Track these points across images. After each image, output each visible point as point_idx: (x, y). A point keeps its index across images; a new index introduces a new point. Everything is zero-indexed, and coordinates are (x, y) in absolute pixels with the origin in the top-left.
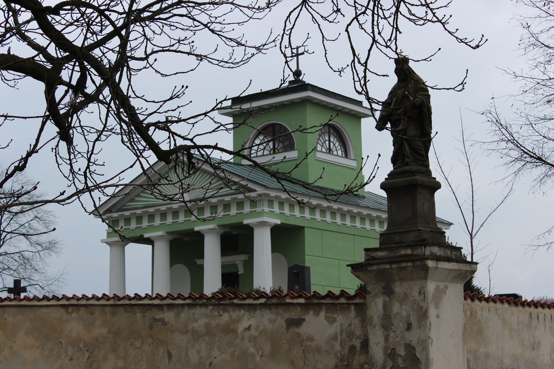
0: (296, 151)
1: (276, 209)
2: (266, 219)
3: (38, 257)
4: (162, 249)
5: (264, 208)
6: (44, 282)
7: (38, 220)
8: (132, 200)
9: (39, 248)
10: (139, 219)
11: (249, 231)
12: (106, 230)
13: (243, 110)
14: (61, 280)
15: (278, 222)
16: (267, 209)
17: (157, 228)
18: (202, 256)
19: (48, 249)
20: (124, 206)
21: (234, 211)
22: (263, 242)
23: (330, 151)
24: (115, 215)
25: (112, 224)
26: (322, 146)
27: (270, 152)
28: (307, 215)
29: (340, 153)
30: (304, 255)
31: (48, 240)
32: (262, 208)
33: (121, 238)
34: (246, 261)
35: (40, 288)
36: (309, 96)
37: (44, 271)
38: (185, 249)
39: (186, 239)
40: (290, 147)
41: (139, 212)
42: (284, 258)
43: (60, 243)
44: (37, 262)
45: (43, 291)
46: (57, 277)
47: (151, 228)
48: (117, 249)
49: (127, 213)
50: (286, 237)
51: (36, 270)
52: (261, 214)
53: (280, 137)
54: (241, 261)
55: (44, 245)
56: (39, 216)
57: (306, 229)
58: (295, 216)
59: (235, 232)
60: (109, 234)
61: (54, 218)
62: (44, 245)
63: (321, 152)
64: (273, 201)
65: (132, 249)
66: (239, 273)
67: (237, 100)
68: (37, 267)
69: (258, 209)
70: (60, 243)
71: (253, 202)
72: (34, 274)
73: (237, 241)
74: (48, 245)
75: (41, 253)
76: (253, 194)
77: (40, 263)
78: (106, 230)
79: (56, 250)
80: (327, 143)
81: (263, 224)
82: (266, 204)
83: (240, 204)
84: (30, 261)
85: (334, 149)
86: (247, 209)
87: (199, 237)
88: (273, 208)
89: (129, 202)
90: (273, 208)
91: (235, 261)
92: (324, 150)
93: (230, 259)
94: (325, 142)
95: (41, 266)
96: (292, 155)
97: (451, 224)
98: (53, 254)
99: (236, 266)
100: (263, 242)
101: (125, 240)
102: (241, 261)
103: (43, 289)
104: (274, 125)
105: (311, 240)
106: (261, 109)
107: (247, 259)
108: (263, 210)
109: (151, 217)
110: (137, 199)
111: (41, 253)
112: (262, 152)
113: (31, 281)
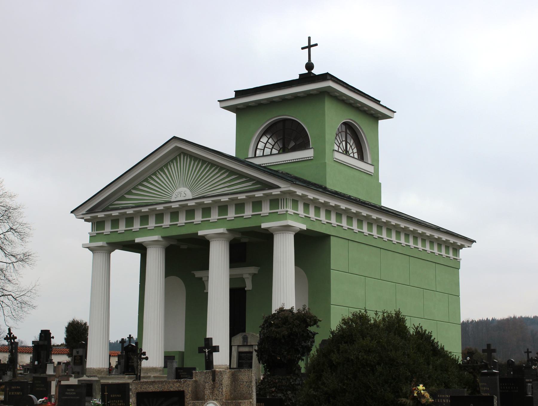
0: (312, 150)
1: (301, 211)
2: (290, 222)
3: (12, 268)
4: (156, 259)
5: (288, 209)
6: (17, 293)
7: (14, 232)
8: (122, 198)
9: (14, 259)
10: (130, 220)
11: (267, 238)
12: (89, 233)
13: (247, 105)
14: (34, 291)
15: (304, 227)
16: (291, 211)
17: (152, 232)
18: (205, 266)
19: (22, 260)
20: (111, 205)
21: (248, 212)
22: (284, 251)
23: (346, 152)
24: (101, 215)
25: (98, 224)
26: (339, 147)
27: (279, 151)
28: (333, 220)
29: (356, 156)
30: (329, 269)
31: (22, 252)
32: (285, 209)
33: (106, 244)
34: (255, 274)
35: (13, 300)
36: (330, 86)
37: (17, 282)
38: (185, 259)
39: (184, 247)
40: (304, 145)
41: (130, 211)
42: (304, 273)
43: (34, 255)
44: (10, 273)
45: (15, 301)
46: (30, 289)
47: (143, 231)
48: (101, 257)
49: (115, 213)
50: (311, 246)
51: (9, 281)
52: (284, 216)
53: (289, 135)
54: (249, 274)
55: (19, 257)
56: (14, 227)
57: (332, 237)
58: (323, 222)
59: (245, 240)
60: (92, 238)
61: (29, 230)
62: (19, 257)
63: (338, 151)
64: (297, 201)
65: (118, 255)
66: (246, 289)
67: (239, 94)
68: (10, 278)
69: (280, 211)
70: (34, 255)
71: (275, 202)
72: (8, 285)
73: (251, 250)
74: (22, 257)
75: (15, 264)
76: (275, 192)
77: (13, 274)
78: (89, 233)
79: (30, 262)
80: (344, 143)
81: (287, 228)
82: (290, 204)
83: (257, 204)
84: (4, 272)
85: (350, 151)
86: (266, 210)
87: (203, 245)
88: (297, 210)
89: (118, 200)
90: (297, 210)
91: (242, 275)
92: (340, 150)
93: (239, 271)
94: (341, 142)
95: (15, 277)
96: (308, 153)
97: (473, 241)
98: (26, 265)
99: (242, 280)
100: (284, 251)
101: (114, 246)
102: (249, 274)
103: (15, 299)
104: (284, 121)
105: (337, 251)
106: (271, 102)
107: (257, 272)
108: (287, 211)
109: (144, 218)
110: (127, 196)
111: (15, 264)
112: (266, 153)
113: (4, 292)
